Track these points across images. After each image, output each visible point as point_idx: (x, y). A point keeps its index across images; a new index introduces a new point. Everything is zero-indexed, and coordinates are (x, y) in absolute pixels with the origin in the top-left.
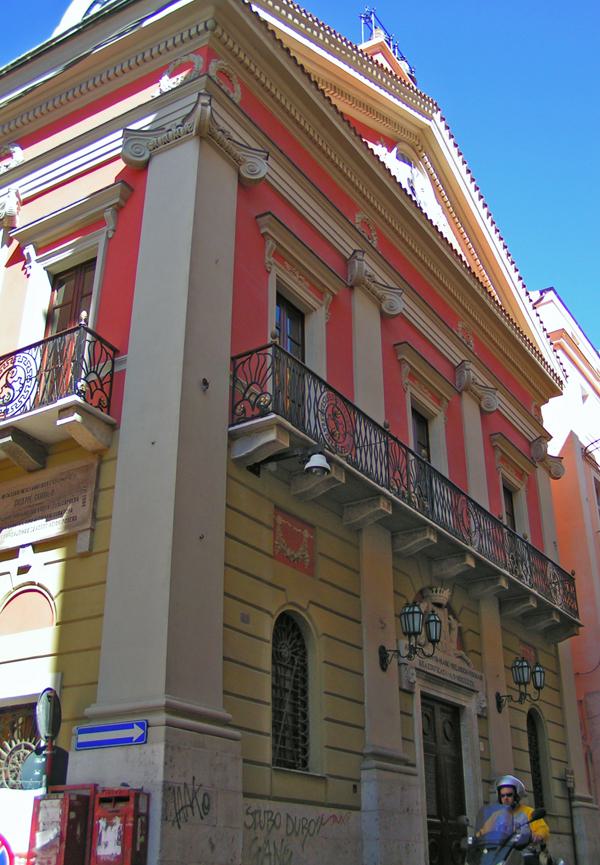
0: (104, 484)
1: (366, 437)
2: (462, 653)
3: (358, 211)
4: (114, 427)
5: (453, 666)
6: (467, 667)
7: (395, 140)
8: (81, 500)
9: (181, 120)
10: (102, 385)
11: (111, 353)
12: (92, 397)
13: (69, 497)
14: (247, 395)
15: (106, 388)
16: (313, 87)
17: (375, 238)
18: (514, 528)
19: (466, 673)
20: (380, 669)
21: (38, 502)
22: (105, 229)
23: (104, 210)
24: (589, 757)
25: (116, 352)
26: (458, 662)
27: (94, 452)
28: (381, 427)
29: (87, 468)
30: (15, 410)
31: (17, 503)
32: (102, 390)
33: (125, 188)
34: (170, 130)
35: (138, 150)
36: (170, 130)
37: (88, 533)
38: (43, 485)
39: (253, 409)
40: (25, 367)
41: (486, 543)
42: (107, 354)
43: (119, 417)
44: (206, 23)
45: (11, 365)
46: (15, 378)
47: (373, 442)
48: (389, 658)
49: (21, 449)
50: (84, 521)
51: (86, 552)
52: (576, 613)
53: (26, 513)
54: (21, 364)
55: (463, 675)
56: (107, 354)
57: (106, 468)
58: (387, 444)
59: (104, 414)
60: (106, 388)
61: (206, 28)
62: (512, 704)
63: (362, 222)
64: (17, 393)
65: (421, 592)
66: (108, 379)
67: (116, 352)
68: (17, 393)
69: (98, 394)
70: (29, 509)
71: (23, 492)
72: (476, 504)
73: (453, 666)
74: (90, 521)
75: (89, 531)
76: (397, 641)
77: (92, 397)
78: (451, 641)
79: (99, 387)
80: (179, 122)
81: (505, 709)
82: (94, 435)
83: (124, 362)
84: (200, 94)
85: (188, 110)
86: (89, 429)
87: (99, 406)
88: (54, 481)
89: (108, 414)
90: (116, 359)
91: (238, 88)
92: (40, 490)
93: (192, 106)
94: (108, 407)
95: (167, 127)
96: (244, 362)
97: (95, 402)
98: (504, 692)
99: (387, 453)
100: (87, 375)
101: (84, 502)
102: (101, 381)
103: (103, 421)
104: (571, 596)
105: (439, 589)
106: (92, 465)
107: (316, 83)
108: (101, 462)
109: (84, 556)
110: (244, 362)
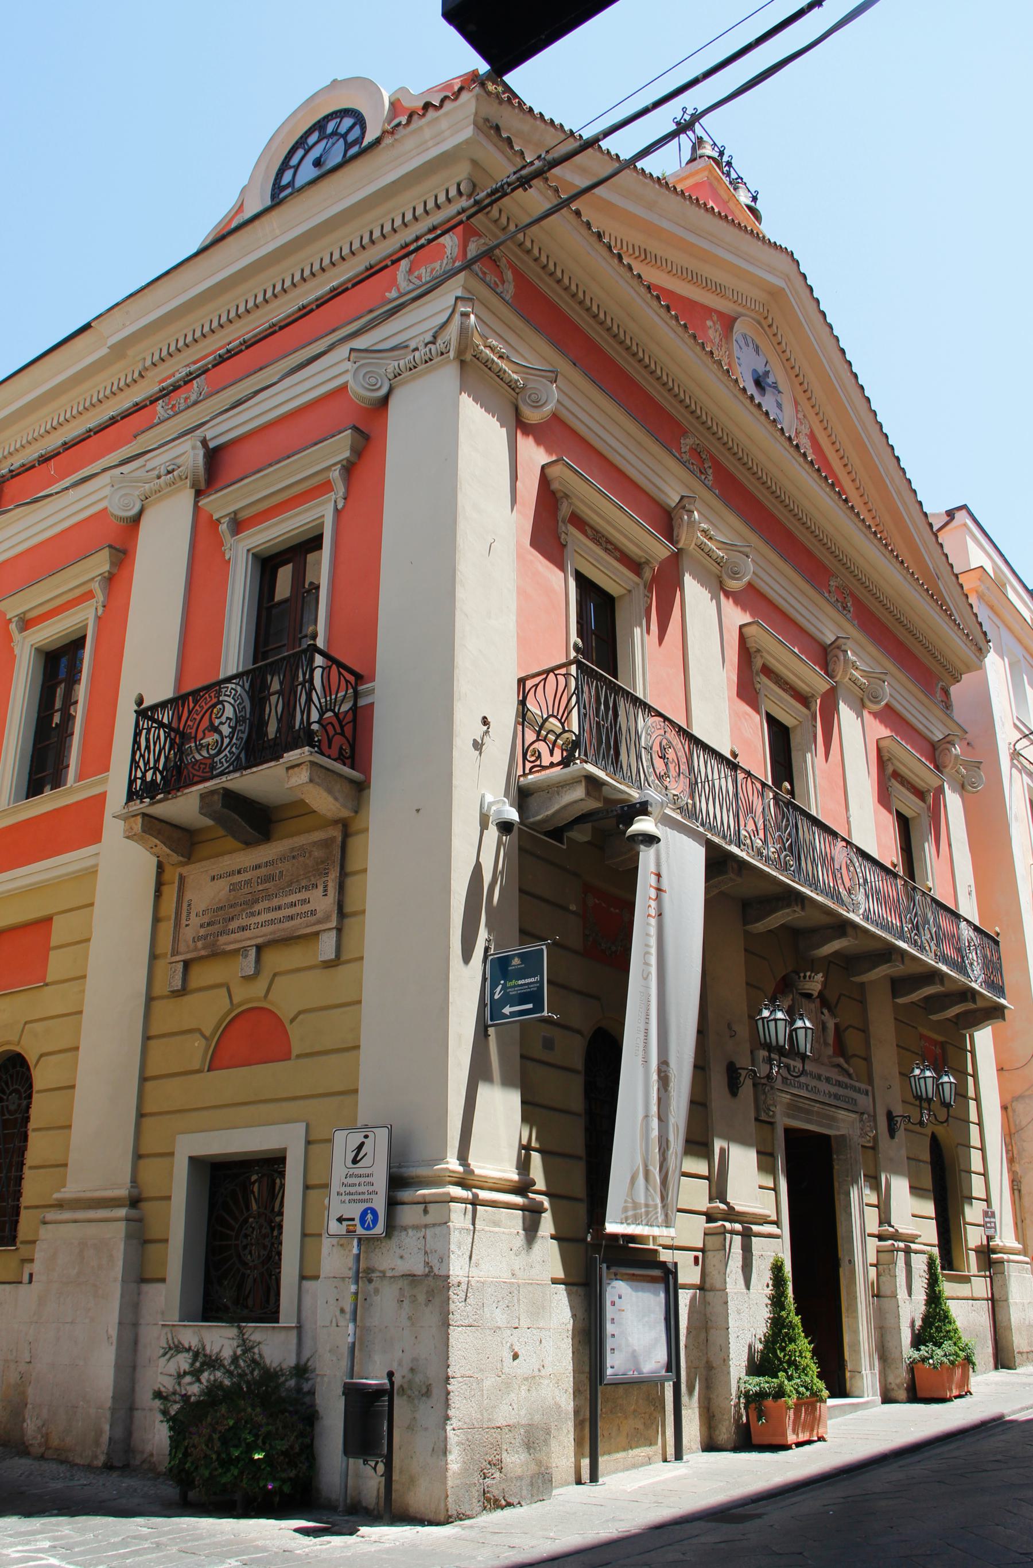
0: (352, 866)
1: (707, 776)
2: (841, 1061)
3: (684, 433)
4: (360, 788)
5: (828, 1080)
6: (846, 1080)
7: (733, 314)
8: (321, 888)
9: (431, 333)
10: (342, 727)
11: (351, 679)
12: (330, 747)
13: (304, 883)
14: (543, 733)
15: (348, 730)
16: (616, 261)
17: (710, 471)
18: (913, 878)
19: (846, 1087)
20: (728, 1095)
21: (260, 888)
22: (332, 495)
23: (328, 468)
24: (371, 311)
25: (359, 678)
26: (834, 1074)
27: (336, 822)
28: (727, 759)
29: (327, 844)
30: (226, 765)
31: (234, 888)
32: (342, 734)
33: (356, 435)
34: (416, 349)
35: (373, 381)
36: (416, 349)
37: (334, 933)
38: (266, 864)
39: (552, 755)
40: (232, 701)
41: (874, 906)
42: (347, 681)
43: (366, 770)
44: (459, 185)
45: (215, 700)
46: (223, 719)
47: (723, 781)
48: (742, 1079)
49: (237, 817)
50: (327, 918)
51: (331, 961)
52: (1000, 991)
53: (246, 903)
54: (226, 698)
55: (841, 1091)
56: (347, 681)
57: (354, 842)
58: (735, 781)
59: (346, 770)
60: (348, 730)
61: (460, 193)
62: (910, 1126)
63: (691, 449)
64: (226, 741)
65: (784, 978)
66: (350, 717)
67: (359, 678)
68: (226, 741)
69: (338, 740)
70: (249, 897)
71: (239, 872)
72: (858, 849)
73: (828, 1080)
74: (335, 916)
75: (334, 932)
76: (752, 1052)
77: (330, 747)
78: (826, 1044)
79: (339, 730)
80: (428, 337)
81: (901, 1134)
82: (336, 799)
83: (372, 691)
84: (457, 298)
85: (443, 318)
86: (330, 791)
87: (341, 758)
88: (282, 859)
89: (353, 767)
90: (360, 688)
91: (509, 275)
92: (263, 871)
93: (450, 311)
94: (352, 757)
95: (413, 345)
96: (537, 685)
97: (334, 752)
98: (898, 1110)
99: (736, 794)
100: (322, 714)
101: (326, 891)
102: (340, 722)
103: (346, 778)
104: (993, 968)
105: (808, 974)
106: (333, 839)
107: (509, 141)
108: (346, 835)
109: (328, 965)
110: (537, 685)
